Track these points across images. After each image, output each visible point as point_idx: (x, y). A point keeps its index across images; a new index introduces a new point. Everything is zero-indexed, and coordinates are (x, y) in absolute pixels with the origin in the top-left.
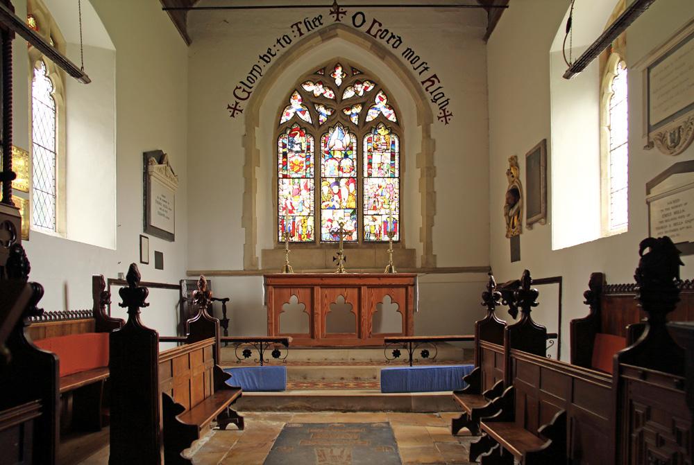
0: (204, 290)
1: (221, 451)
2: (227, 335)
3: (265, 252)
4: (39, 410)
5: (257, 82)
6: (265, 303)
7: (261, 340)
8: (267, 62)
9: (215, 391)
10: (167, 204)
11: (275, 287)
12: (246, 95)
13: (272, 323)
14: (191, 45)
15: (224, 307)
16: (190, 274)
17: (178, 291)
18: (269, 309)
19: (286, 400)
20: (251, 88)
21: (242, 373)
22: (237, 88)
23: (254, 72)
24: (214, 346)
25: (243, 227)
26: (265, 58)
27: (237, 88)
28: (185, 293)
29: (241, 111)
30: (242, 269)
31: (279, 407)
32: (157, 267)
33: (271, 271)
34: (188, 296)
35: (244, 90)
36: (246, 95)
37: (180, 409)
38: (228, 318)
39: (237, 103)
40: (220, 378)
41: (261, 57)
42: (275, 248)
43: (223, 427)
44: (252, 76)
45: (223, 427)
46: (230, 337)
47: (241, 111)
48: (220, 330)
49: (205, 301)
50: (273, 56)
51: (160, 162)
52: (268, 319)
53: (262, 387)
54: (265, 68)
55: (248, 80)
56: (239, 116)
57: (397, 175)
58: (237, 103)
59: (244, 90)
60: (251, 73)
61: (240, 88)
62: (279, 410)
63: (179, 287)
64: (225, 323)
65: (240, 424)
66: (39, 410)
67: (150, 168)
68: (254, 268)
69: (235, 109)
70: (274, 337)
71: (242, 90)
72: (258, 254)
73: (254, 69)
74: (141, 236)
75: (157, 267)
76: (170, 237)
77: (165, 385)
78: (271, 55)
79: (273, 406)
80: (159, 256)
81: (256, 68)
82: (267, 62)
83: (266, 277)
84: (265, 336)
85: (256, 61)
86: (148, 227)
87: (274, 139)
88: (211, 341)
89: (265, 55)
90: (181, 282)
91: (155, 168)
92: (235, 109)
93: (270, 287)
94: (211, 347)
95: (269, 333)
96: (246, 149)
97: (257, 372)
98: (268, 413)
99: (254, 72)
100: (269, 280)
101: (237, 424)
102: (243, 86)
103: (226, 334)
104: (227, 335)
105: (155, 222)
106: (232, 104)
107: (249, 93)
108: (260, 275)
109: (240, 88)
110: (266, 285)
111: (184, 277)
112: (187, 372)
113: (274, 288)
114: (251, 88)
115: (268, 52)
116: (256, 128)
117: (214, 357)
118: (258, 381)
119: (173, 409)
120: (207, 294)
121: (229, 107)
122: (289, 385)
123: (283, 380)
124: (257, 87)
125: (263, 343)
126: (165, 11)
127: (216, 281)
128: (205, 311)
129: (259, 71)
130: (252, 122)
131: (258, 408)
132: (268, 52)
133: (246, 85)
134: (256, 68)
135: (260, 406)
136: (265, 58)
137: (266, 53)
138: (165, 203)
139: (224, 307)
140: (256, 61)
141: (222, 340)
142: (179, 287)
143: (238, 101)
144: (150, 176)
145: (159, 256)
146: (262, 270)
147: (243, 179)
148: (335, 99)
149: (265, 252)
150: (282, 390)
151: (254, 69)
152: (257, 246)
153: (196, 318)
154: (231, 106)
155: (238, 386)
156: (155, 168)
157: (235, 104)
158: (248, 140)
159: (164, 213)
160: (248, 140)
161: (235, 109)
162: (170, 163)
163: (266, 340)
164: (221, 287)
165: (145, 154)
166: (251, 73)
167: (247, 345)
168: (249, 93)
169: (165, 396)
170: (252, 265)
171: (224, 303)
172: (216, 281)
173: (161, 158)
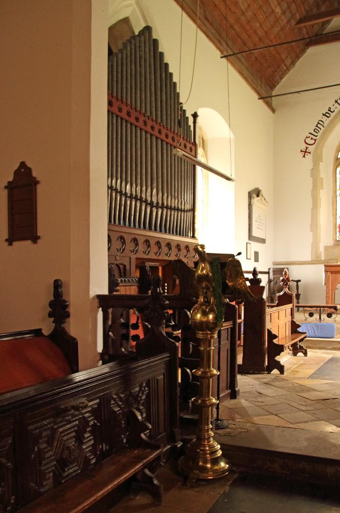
0: (287, 277)
1: (295, 364)
2: (299, 303)
3: (326, 248)
4: (232, 325)
5: (321, 132)
6: (325, 284)
7: (320, 307)
8: (328, 117)
9: (292, 334)
10: (261, 221)
11: (332, 273)
12: (313, 142)
13: (329, 297)
14: (276, 113)
15: (297, 286)
16: (275, 264)
17: (267, 275)
18: (327, 287)
19: (334, 343)
20: (316, 136)
21: (307, 326)
22: (307, 137)
23: (319, 125)
24: (292, 309)
25: (311, 231)
26: (327, 114)
27: (307, 137)
28: (272, 277)
29: (310, 153)
30: (310, 260)
31: (329, 348)
32: (255, 261)
33: (330, 261)
34: (274, 278)
35: (312, 139)
36: (313, 141)
37: (275, 337)
38: (299, 293)
39: (307, 148)
40: (294, 327)
41: (323, 115)
42: (334, 245)
43: (295, 354)
44: (317, 128)
45: (295, 354)
46: (300, 305)
47: (310, 153)
48: (295, 300)
49: (287, 283)
50: (332, 112)
51: (258, 196)
52: (327, 294)
53: (320, 336)
54: (327, 121)
55: (314, 131)
56: (308, 156)
57: (242, 344)
58: (307, 148)
59: (312, 139)
60: (317, 126)
61: (309, 137)
62: (330, 349)
63: (268, 273)
64: (298, 296)
65: (305, 354)
66: (232, 325)
67: (253, 201)
68: (318, 259)
69: (306, 152)
70: (330, 305)
71: (310, 138)
72: (322, 249)
73: (318, 123)
74: (247, 243)
75: (255, 261)
76: (263, 241)
77: (268, 326)
78: (331, 112)
79: (326, 346)
80: (256, 254)
81: (320, 122)
82: (328, 117)
83: (326, 266)
84: (324, 304)
85: (320, 117)
86: (251, 237)
87: (334, 168)
88: (290, 306)
89: (326, 113)
90: (269, 269)
91: (255, 200)
92: (305, 152)
93: (329, 273)
94: (290, 309)
95: (327, 304)
96: (314, 179)
97: (317, 326)
98: (322, 351)
99: (319, 125)
100: (328, 268)
101: (303, 353)
102: (311, 136)
103: (298, 303)
104: (299, 303)
105: (254, 234)
106: (303, 148)
107: (315, 140)
108: (322, 263)
109: (309, 137)
110: (326, 271)
111: (272, 266)
112: (277, 321)
113: (332, 273)
114: (316, 136)
115: (329, 110)
116: (321, 163)
117: (291, 315)
118: (318, 332)
119: (272, 336)
120: (288, 279)
121: (302, 151)
122: (335, 337)
123: (334, 335)
124: (321, 135)
125: (322, 308)
126: (260, 100)
127: (291, 267)
128: (287, 289)
129: (323, 124)
130: (317, 160)
131: (317, 348)
132: (329, 110)
133: (313, 135)
134: (320, 122)
135: (318, 346)
136: (327, 114)
137: (327, 111)
138: (260, 221)
139: (297, 286)
140: (320, 117)
141: (296, 306)
142: (268, 273)
143: (307, 146)
144: (252, 205)
145: (256, 254)
146: (324, 260)
147: (311, 199)
148: (211, 468)
149: (326, 248)
150: (333, 338)
151: (318, 123)
152: (321, 244)
153: (282, 293)
154: (303, 150)
155: (304, 332)
156: (255, 200)
157: (305, 148)
158: (315, 172)
159: (260, 227)
160: (315, 172)
161: (306, 152)
162: (264, 195)
163: (324, 307)
164: (295, 273)
165: (249, 193)
166: (317, 126)
167: (312, 310)
168: (315, 140)
169: (268, 330)
170: (317, 257)
171: (297, 283)
172: (291, 267)
173: (258, 193)
